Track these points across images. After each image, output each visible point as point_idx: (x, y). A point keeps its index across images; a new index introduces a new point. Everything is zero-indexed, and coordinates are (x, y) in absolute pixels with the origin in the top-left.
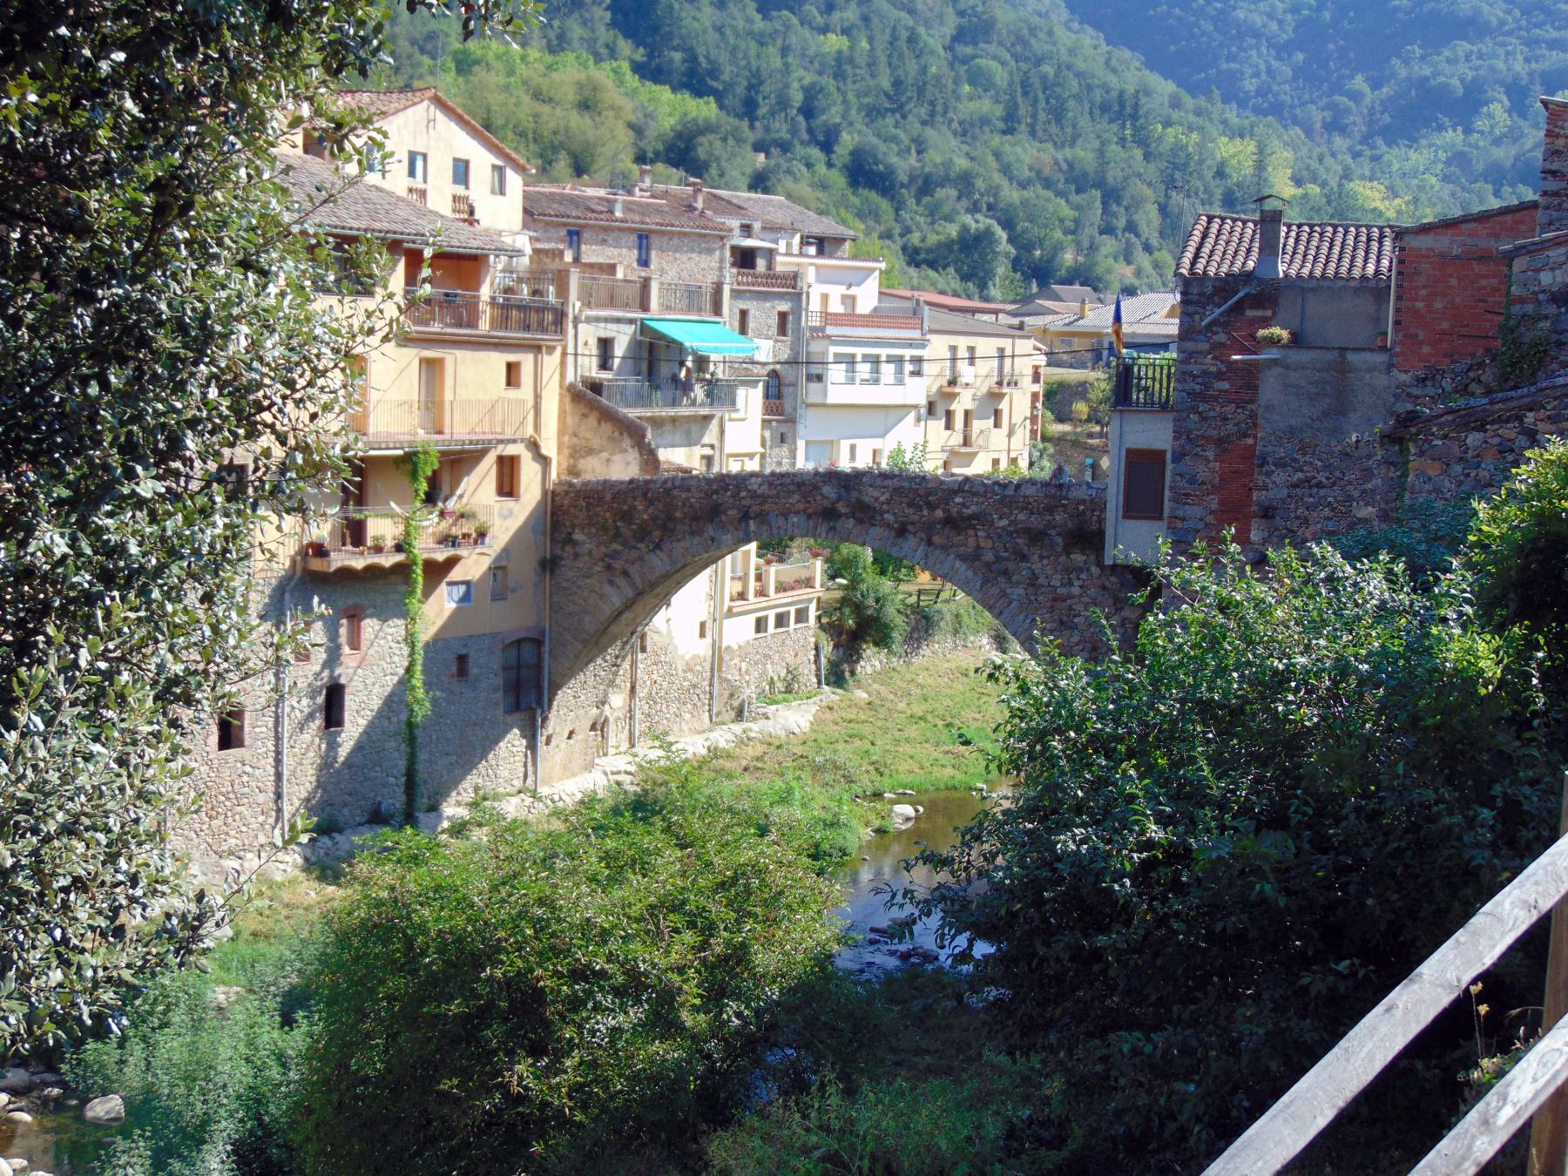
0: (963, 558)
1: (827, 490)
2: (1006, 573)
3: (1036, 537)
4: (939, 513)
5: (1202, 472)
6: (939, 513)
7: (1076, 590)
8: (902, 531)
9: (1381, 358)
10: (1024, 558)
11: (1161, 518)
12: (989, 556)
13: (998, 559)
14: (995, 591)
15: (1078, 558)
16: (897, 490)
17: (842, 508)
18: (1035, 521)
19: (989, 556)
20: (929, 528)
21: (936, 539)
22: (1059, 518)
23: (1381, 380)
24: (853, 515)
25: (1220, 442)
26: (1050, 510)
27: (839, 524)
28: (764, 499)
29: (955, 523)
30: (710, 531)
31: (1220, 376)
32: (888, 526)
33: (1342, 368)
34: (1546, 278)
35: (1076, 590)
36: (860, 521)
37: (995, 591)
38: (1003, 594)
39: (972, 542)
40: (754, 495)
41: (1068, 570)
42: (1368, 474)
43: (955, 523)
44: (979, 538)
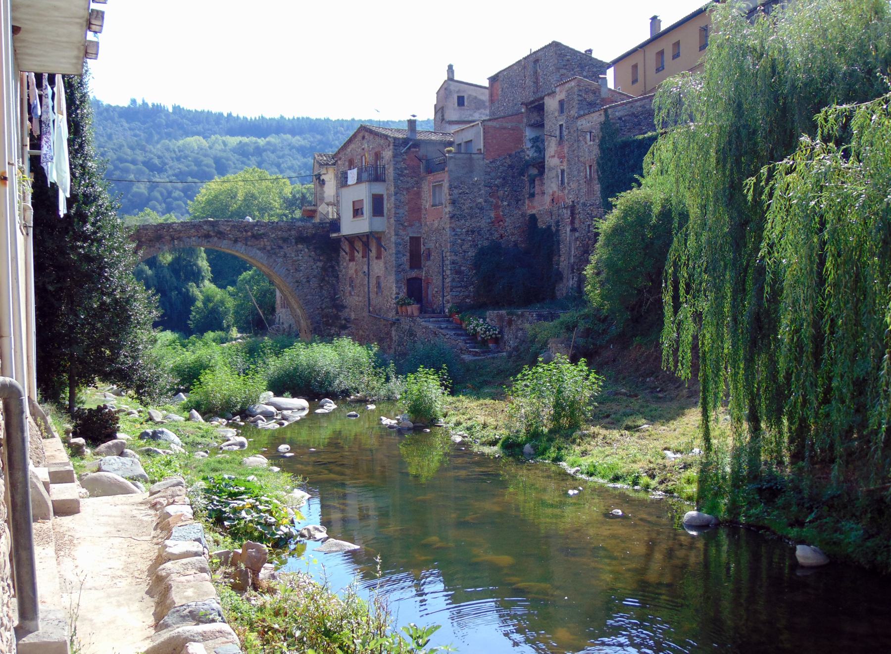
0: (259, 249)
1: (205, 227)
2: (275, 254)
3: (285, 240)
4: (249, 234)
5: (402, 198)
6: (249, 234)
7: (300, 258)
8: (236, 241)
9: (481, 156)
10: (282, 248)
11: (383, 216)
12: (269, 248)
13: (272, 249)
14: (272, 260)
15: (300, 246)
16: (233, 226)
17: (212, 233)
18: (285, 235)
19: (269, 248)
20: (246, 239)
21: (249, 243)
22: (293, 232)
23: (482, 163)
24: (216, 236)
25: (407, 189)
26: (290, 230)
27: (211, 240)
28: (180, 232)
29: (256, 237)
30: (158, 245)
31: (406, 169)
32: (230, 239)
33: (471, 159)
34: (617, 114)
35: (300, 258)
36: (219, 238)
37: (272, 260)
38: (275, 261)
39: (262, 243)
40: (175, 230)
41: (297, 251)
42: (480, 189)
43: (256, 237)
44: (265, 242)
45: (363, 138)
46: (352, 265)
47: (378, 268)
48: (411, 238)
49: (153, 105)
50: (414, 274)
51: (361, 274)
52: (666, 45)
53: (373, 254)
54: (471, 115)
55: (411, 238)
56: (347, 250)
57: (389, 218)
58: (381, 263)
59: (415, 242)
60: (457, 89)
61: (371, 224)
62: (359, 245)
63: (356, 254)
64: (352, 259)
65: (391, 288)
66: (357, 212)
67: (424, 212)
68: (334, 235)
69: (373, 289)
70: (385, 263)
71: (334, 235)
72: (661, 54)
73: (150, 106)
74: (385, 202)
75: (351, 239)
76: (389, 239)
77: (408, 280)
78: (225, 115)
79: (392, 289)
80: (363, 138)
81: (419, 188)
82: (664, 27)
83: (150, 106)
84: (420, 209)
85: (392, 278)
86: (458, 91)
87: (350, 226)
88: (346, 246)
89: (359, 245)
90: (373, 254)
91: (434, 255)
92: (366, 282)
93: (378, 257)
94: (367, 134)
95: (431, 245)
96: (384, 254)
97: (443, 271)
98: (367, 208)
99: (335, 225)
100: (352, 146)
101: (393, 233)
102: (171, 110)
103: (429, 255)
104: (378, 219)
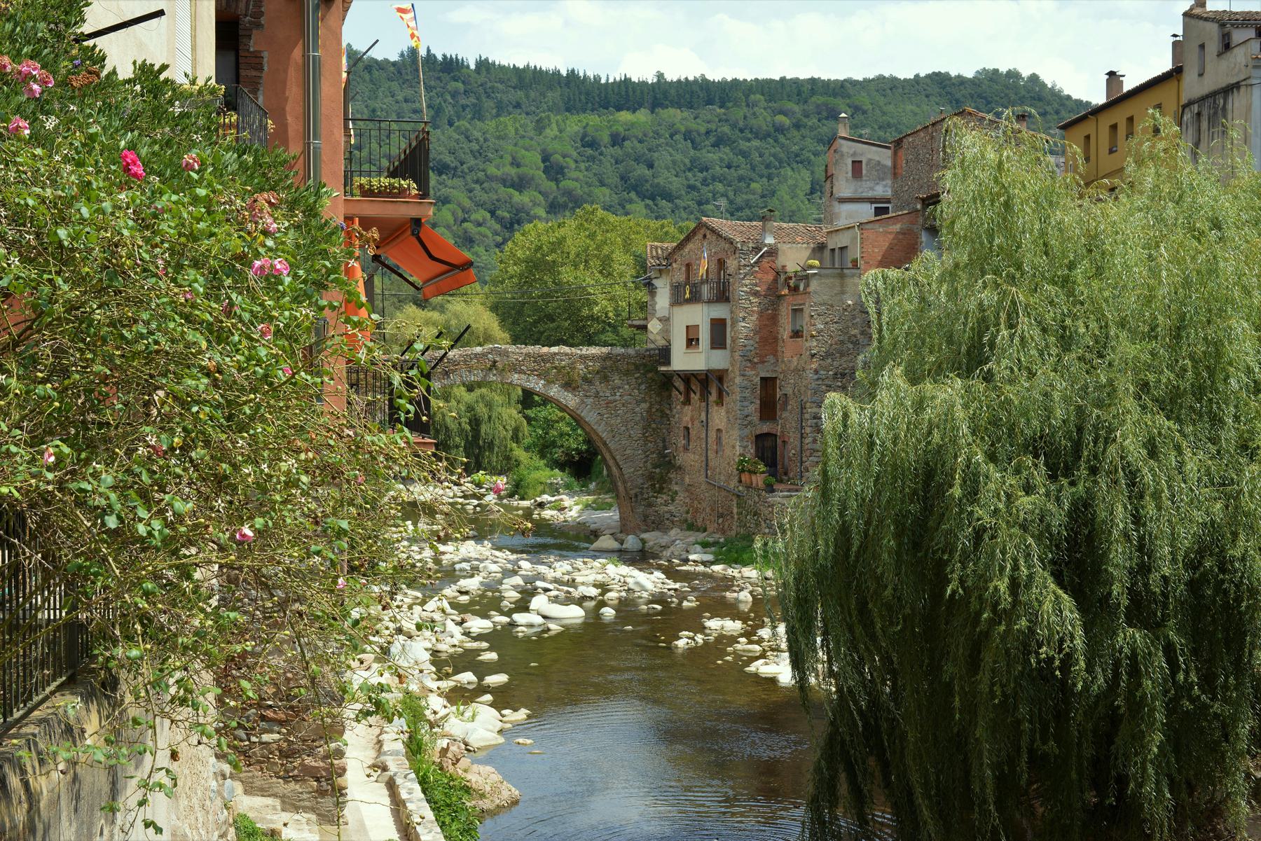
7: (617, 397)
35: (617, 397)
41: (613, 389)
45: (705, 236)
46: (687, 409)
47: (719, 417)
48: (762, 378)
49: (444, 56)
50: (765, 428)
51: (697, 423)
52: (1119, 116)
53: (713, 397)
54: (872, 189)
55: (762, 378)
56: (682, 388)
57: (733, 351)
58: (723, 411)
59: (768, 384)
60: (851, 152)
61: (708, 359)
62: (695, 386)
63: (692, 395)
64: (687, 401)
65: (734, 447)
66: (692, 342)
67: (780, 343)
68: (663, 368)
69: (713, 446)
70: (727, 412)
71: (663, 368)
72: (1114, 127)
73: (440, 58)
74: (728, 329)
75: (688, 377)
76: (733, 380)
77: (758, 437)
78: (564, 73)
79: (737, 446)
80: (705, 236)
81: (775, 310)
82: (1128, 85)
83: (440, 58)
84: (776, 339)
85: (736, 433)
86: (854, 154)
87: (683, 360)
88: (679, 384)
89: (695, 386)
90: (713, 397)
91: (792, 404)
92: (703, 436)
93: (720, 401)
94: (708, 232)
95: (789, 390)
96: (726, 399)
97: (802, 427)
98: (704, 336)
99: (665, 354)
100: (690, 246)
101: (738, 373)
102: (473, 67)
103: (786, 403)
104: (718, 353)
